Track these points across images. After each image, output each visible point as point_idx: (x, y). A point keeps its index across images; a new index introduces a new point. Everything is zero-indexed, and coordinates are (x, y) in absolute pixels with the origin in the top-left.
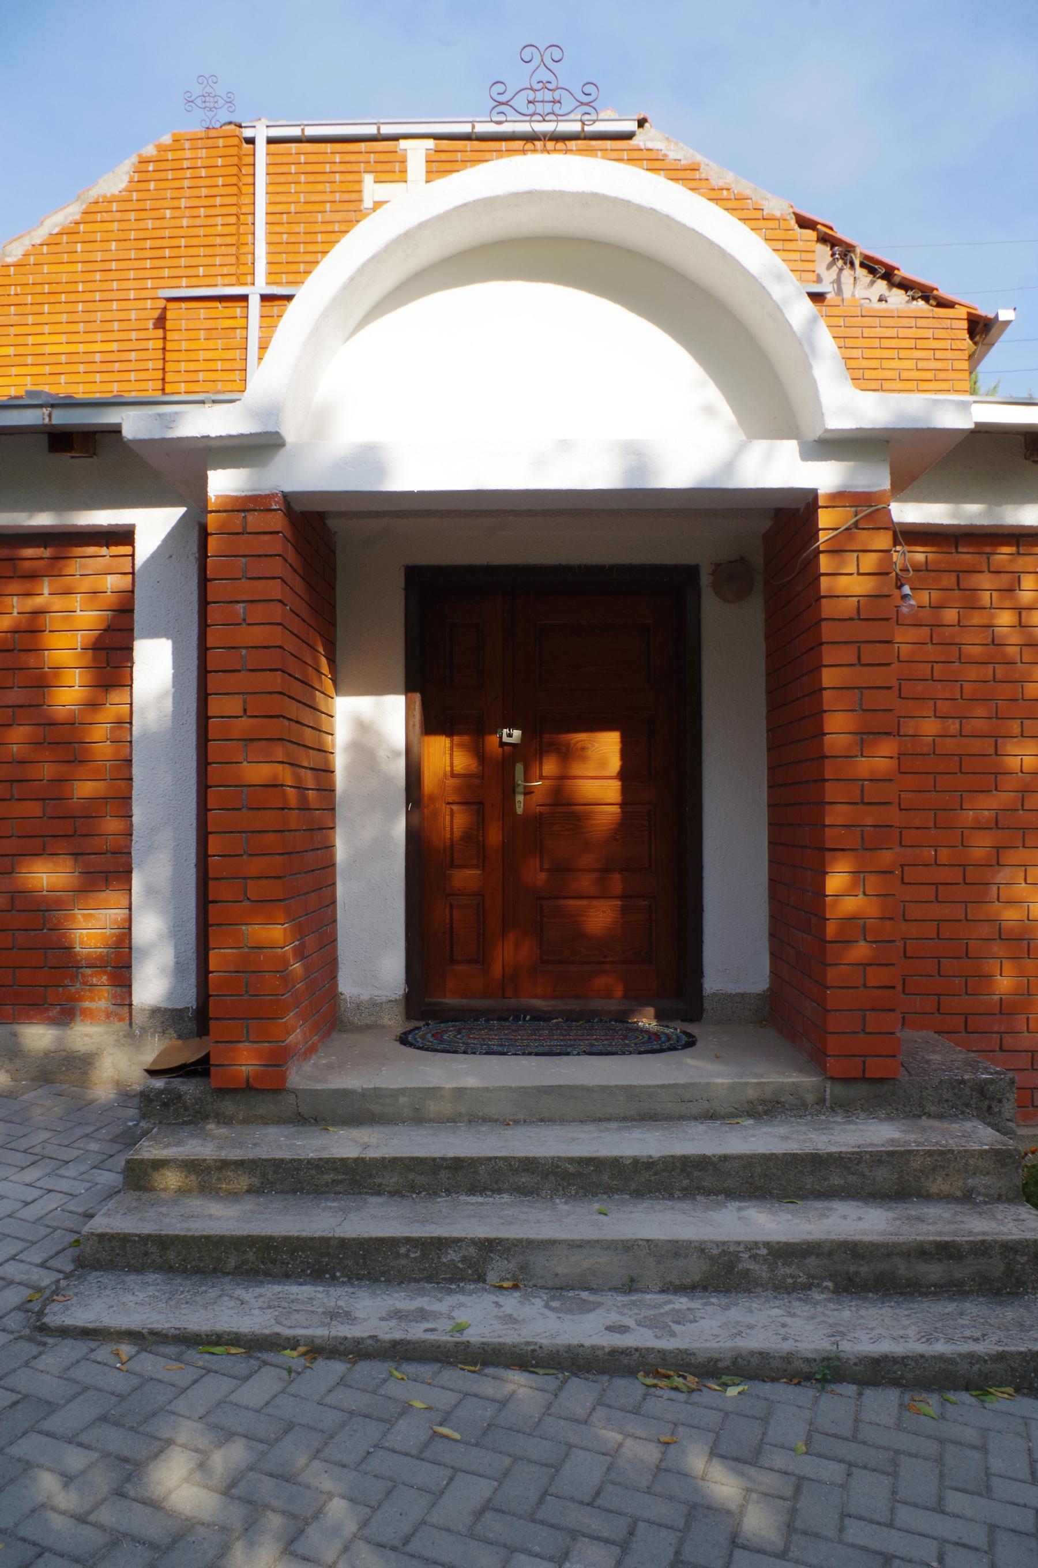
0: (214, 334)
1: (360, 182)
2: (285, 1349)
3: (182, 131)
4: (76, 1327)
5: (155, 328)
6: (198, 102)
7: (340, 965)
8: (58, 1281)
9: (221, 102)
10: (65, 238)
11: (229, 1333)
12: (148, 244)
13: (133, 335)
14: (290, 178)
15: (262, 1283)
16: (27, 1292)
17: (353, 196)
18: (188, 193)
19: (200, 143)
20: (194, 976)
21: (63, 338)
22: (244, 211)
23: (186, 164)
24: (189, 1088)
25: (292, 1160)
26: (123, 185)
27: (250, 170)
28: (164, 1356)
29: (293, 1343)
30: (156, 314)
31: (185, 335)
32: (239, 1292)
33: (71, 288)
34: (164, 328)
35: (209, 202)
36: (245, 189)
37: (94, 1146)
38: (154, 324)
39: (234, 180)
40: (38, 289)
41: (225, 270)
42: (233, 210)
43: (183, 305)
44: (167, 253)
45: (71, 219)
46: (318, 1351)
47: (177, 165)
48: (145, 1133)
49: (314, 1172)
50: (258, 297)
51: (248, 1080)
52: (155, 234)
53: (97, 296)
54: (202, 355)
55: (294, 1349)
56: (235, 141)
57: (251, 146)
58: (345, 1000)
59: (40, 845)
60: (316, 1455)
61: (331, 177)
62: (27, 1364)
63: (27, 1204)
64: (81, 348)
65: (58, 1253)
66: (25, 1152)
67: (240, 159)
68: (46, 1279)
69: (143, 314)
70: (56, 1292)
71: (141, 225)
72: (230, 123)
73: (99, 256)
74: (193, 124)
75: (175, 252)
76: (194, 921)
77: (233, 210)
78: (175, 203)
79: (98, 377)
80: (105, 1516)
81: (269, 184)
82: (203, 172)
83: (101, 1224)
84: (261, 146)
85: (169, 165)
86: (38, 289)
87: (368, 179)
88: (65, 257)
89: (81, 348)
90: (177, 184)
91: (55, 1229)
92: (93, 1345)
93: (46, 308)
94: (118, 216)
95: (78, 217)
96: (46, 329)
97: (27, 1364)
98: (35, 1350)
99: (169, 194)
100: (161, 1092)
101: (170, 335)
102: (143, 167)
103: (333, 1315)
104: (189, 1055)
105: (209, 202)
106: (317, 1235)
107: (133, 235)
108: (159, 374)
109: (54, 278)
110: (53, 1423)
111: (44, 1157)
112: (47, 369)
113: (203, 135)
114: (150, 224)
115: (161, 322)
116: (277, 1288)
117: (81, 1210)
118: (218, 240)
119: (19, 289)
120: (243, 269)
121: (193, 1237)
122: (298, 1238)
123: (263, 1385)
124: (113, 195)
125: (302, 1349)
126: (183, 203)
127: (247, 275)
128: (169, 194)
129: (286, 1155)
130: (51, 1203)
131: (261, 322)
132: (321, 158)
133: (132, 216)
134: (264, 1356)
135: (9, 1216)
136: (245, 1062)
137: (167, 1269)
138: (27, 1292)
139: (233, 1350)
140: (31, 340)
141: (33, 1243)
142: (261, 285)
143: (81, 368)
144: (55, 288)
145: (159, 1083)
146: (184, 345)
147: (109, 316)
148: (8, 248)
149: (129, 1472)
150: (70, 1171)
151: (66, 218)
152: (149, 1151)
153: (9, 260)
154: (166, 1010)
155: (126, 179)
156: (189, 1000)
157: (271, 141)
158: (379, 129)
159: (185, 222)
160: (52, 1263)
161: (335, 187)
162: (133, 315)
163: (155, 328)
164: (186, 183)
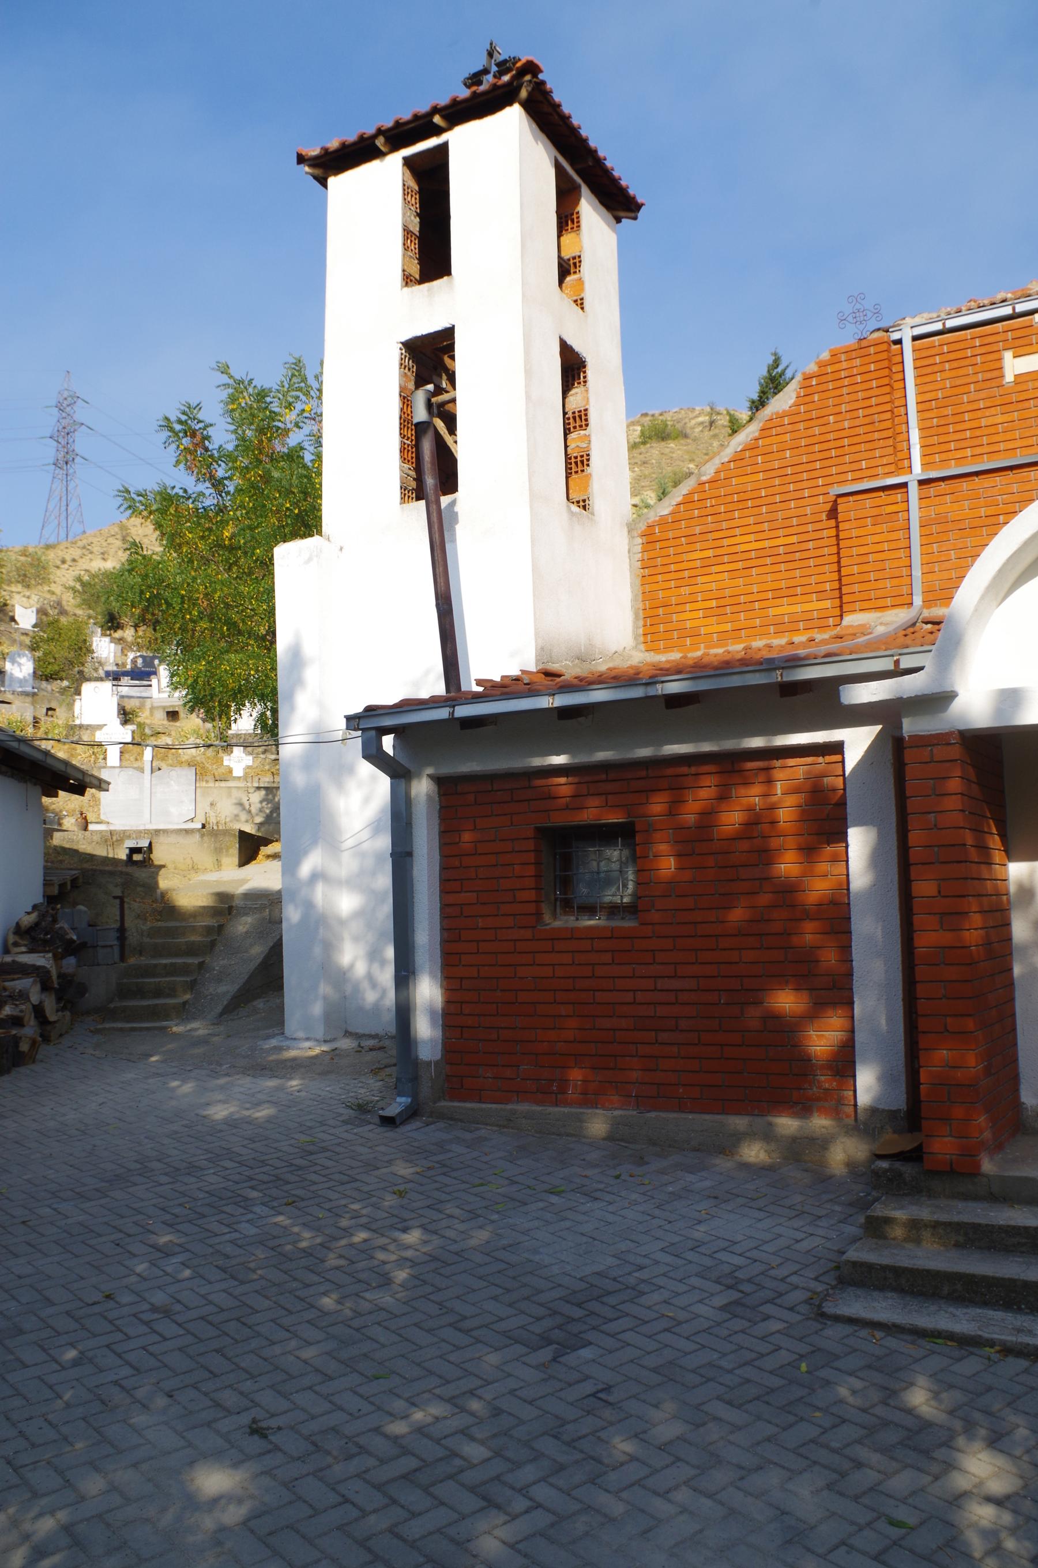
0: (879, 519)
1: (1000, 359)
2: (985, 1346)
3: (838, 346)
4: (844, 1316)
5: (828, 519)
6: (850, 319)
7: (1022, 1080)
8: (827, 1290)
9: (869, 314)
10: (747, 454)
11: (947, 1331)
12: (817, 448)
13: (810, 527)
14: (936, 368)
15: (967, 1307)
16: (809, 1294)
17: (995, 374)
18: (847, 398)
19: (854, 354)
20: (904, 1086)
21: (752, 537)
22: (896, 404)
23: (843, 374)
24: (908, 1170)
25: (987, 1225)
26: (791, 402)
27: (899, 368)
28: (905, 1341)
29: (991, 1343)
30: (828, 506)
31: (854, 524)
32: (951, 1309)
33: (755, 494)
34: (836, 518)
35: (867, 403)
36: (896, 385)
37: (837, 1208)
38: (827, 516)
39: (886, 381)
40: (729, 499)
41: (885, 461)
42: (888, 407)
43: (851, 498)
44: (833, 453)
45: (751, 436)
46: (1008, 1351)
47: (836, 376)
48: (876, 1200)
49: (1003, 1235)
50: (916, 483)
51: (951, 1165)
52: (823, 438)
53: (778, 498)
54: (870, 539)
55: (992, 1347)
56: (884, 347)
57: (898, 346)
58: (1026, 1108)
59: (780, 978)
60: (1009, 1404)
61: (973, 361)
62: (816, 1333)
63: (798, 1241)
64: (766, 544)
65: (824, 1273)
66: (789, 1208)
67: (890, 361)
68: (820, 1288)
69: (817, 508)
70: (828, 1295)
71: (810, 432)
72: (878, 330)
73: (776, 464)
74: (847, 338)
75: (840, 452)
76: (903, 1043)
77: (888, 407)
78: (837, 409)
79: (783, 567)
80: (879, 1410)
81: (916, 377)
82: (859, 379)
83: (853, 1254)
84: (908, 345)
85: (830, 377)
86: (729, 499)
87: (1008, 355)
88: (749, 470)
89: (766, 544)
90: (838, 392)
91: (820, 1258)
92: (856, 1328)
93: (737, 514)
94: (790, 428)
95: (757, 434)
96: (737, 531)
97: (816, 1333)
98: (820, 1326)
99: (831, 402)
100: (887, 1170)
101: (842, 526)
102: (807, 383)
103: (1019, 1331)
104: (906, 1143)
105: (867, 403)
106: (1007, 1276)
107: (803, 442)
108: (835, 558)
109: (741, 488)
110: (836, 1364)
111: (804, 1212)
112: (740, 565)
113: (856, 347)
114: (817, 431)
115: (833, 513)
116: (979, 1311)
117: (836, 1248)
118: (876, 435)
119: (713, 502)
120: (900, 456)
121: (917, 1270)
122: (993, 1278)
123: (971, 1365)
124: (784, 411)
125: (997, 1348)
126: (843, 408)
127: (903, 463)
128: (831, 402)
129: (983, 1221)
130: (818, 1241)
131: (920, 504)
132: (962, 345)
133: (801, 426)
134: (971, 1349)
135: (788, 1248)
136: (943, 1146)
137: (900, 1290)
138: (809, 1294)
139: (949, 1343)
140: (726, 542)
141: (807, 1266)
142: (918, 470)
143: (768, 560)
144: (743, 496)
145: (884, 1165)
146: (856, 569)
147: (789, 514)
148: (703, 469)
149: (890, 1395)
150: (823, 1223)
151: (747, 437)
152: (879, 1210)
153: (704, 478)
154: (883, 1111)
155: (794, 395)
156: (899, 1101)
157: (915, 338)
158: (1014, 309)
159: (846, 424)
160: (820, 1279)
161: (977, 369)
162: (808, 510)
163: (828, 519)
164: (845, 390)
